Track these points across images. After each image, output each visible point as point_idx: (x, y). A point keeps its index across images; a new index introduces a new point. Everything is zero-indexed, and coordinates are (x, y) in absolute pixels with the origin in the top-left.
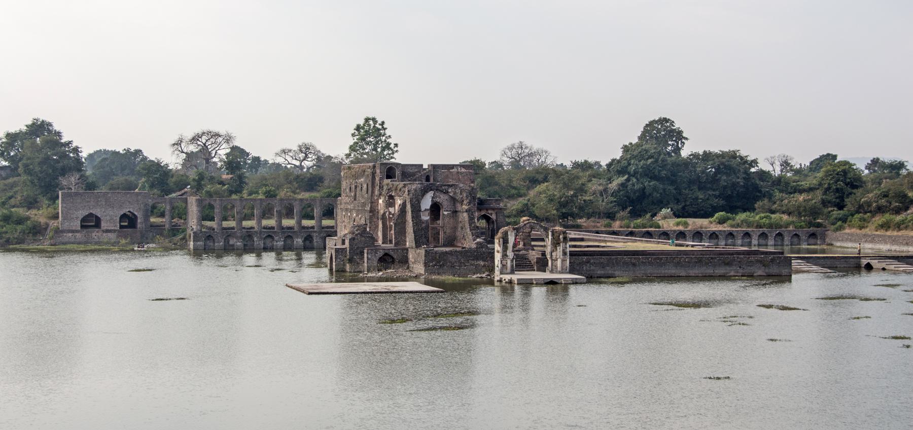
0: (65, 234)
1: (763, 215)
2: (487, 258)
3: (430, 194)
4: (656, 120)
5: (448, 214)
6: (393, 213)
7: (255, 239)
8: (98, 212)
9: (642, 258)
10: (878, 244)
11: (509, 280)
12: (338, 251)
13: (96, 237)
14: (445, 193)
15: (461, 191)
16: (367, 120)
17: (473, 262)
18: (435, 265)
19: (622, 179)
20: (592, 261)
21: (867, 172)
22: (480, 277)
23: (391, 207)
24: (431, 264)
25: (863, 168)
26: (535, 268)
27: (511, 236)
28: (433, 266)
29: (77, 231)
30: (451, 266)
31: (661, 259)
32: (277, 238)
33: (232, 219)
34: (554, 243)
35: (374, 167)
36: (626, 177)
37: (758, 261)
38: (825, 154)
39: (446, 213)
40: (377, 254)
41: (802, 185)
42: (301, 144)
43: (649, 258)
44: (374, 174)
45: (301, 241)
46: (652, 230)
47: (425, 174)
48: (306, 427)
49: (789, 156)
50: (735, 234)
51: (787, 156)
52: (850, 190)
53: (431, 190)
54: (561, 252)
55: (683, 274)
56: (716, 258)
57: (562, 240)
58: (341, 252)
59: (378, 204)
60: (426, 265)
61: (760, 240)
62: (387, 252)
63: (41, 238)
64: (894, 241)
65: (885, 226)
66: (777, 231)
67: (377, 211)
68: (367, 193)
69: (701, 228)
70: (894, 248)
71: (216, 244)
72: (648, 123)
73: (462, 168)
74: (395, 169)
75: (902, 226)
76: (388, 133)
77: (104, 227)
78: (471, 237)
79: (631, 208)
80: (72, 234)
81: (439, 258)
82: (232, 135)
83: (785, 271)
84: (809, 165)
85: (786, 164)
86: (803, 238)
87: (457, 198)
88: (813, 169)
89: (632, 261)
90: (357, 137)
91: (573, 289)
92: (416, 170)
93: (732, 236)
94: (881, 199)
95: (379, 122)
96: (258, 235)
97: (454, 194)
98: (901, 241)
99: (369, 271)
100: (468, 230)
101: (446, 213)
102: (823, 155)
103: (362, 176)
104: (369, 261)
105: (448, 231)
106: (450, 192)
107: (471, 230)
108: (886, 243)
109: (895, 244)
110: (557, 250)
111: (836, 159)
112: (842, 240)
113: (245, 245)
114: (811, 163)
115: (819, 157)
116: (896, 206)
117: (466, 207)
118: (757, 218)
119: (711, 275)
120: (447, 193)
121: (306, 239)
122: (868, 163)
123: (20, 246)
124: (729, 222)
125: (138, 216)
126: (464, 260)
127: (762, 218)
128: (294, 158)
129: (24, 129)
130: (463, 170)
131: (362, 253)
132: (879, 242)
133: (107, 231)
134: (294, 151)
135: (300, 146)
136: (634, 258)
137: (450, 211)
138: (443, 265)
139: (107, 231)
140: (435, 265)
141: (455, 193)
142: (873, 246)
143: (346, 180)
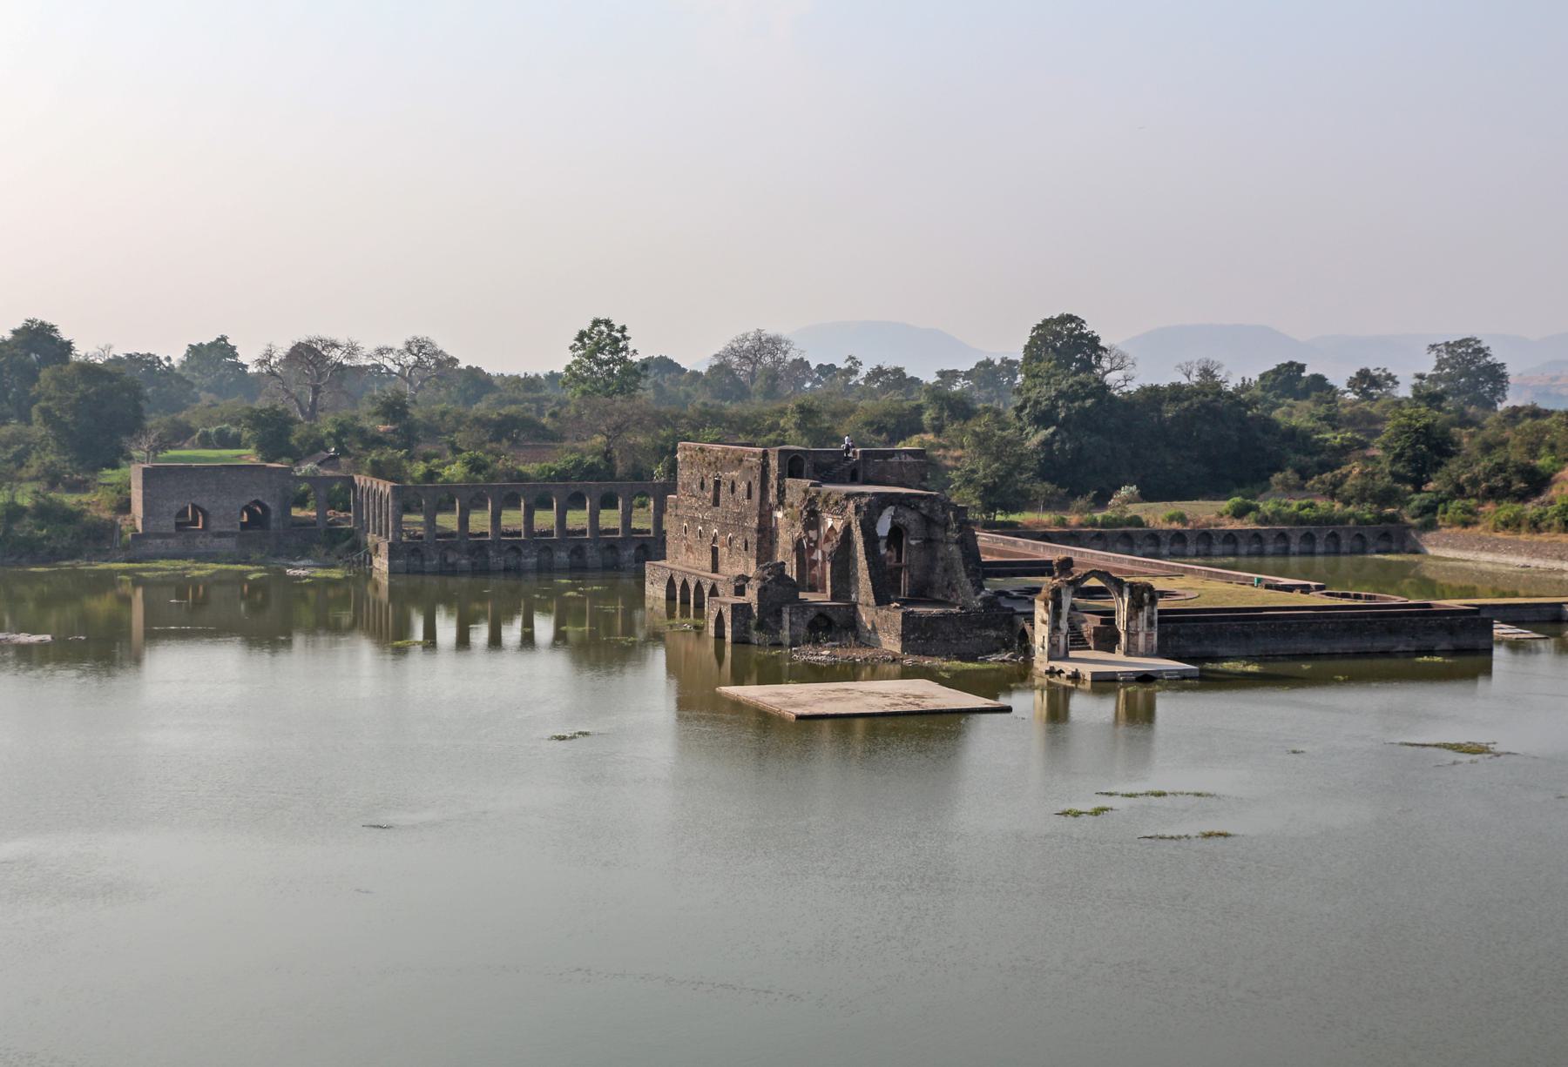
0: (150, 541)
1: (1304, 502)
2: (1001, 624)
4: (1055, 317)
5: (917, 544)
6: (815, 539)
7: (491, 553)
8: (204, 502)
9: (1261, 624)
10: (1505, 556)
11: (1073, 672)
12: (737, 608)
13: (201, 546)
14: (912, 509)
15: (943, 508)
16: (596, 323)
17: (978, 632)
18: (919, 638)
19: (1044, 434)
20: (1182, 631)
21: (1351, 396)
22: (1001, 661)
23: (813, 530)
24: (912, 637)
25: (1341, 385)
26: (1092, 644)
27: (1066, 595)
28: (915, 640)
29: (169, 536)
30: (945, 640)
31: (1290, 626)
32: (527, 551)
33: (419, 509)
34: (1133, 605)
35: (765, 454)
36: (1051, 430)
37: (1441, 626)
38: (1286, 362)
39: (913, 543)
40: (806, 614)
41: (1327, 440)
42: (411, 340)
43: (1271, 624)
44: (765, 468)
45: (566, 557)
46: (1132, 531)
47: (850, 466)
49: (1216, 361)
50: (1264, 535)
51: (1213, 362)
52: (1437, 458)
53: (892, 504)
54: (1145, 621)
55: (1324, 650)
56: (1375, 622)
57: (1147, 601)
58: (742, 610)
59: (771, 519)
60: (904, 638)
61: (1302, 545)
62: (822, 610)
63: (108, 547)
64: (1534, 551)
65: (1513, 524)
66: (1329, 529)
67: (769, 529)
68: (749, 497)
69: (1210, 525)
70: (1536, 562)
71: (427, 563)
72: (1041, 323)
73: (907, 456)
74: (802, 460)
75: (1542, 525)
76: (631, 346)
77: (214, 527)
78: (969, 587)
79: (1095, 492)
80: (161, 541)
81: (926, 625)
82: (357, 345)
83: (1482, 643)
84: (1257, 379)
86: (1371, 540)
87: (936, 518)
88: (1267, 388)
89: (1245, 630)
90: (581, 352)
92: (833, 460)
93: (1257, 539)
94: (1493, 475)
95: (617, 327)
96: (496, 546)
97: (930, 512)
98: (1548, 553)
100: (963, 574)
101: (913, 543)
102: (1283, 364)
103: (735, 469)
104: (793, 627)
105: (916, 573)
106: (922, 509)
107: (968, 576)
108: (1519, 554)
109: (1537, 557)
110: (1137, 617)
111: (1304, 371)
112: (1437, 545)
113: (474, 564)
114: (1263, 377)
115: (1275, 367)
116: (1520, 489)
117: (956, 536)
118: (1295, 504)
119: (1367, 650)
120: (917, 508)
121: (573, 552)
122: (1351, 378)
124: (1252, 514)
125: (272, 508)
126: (965, 629)
127: (1302, 508)
128: (397, 362)
129: (8, 336)
130: (910, 459)
131: (779, 613)
132: (1508, 552)
133: (220, 535)
134: (398, 351)
135: (409, 343)
136: (1248, 625)
137: (921, 539)
138: (932, 637)
139: (220, 535)
140: (919, 638)
141: (932, 510)
142: (1496, 558)
143: (691, 468)
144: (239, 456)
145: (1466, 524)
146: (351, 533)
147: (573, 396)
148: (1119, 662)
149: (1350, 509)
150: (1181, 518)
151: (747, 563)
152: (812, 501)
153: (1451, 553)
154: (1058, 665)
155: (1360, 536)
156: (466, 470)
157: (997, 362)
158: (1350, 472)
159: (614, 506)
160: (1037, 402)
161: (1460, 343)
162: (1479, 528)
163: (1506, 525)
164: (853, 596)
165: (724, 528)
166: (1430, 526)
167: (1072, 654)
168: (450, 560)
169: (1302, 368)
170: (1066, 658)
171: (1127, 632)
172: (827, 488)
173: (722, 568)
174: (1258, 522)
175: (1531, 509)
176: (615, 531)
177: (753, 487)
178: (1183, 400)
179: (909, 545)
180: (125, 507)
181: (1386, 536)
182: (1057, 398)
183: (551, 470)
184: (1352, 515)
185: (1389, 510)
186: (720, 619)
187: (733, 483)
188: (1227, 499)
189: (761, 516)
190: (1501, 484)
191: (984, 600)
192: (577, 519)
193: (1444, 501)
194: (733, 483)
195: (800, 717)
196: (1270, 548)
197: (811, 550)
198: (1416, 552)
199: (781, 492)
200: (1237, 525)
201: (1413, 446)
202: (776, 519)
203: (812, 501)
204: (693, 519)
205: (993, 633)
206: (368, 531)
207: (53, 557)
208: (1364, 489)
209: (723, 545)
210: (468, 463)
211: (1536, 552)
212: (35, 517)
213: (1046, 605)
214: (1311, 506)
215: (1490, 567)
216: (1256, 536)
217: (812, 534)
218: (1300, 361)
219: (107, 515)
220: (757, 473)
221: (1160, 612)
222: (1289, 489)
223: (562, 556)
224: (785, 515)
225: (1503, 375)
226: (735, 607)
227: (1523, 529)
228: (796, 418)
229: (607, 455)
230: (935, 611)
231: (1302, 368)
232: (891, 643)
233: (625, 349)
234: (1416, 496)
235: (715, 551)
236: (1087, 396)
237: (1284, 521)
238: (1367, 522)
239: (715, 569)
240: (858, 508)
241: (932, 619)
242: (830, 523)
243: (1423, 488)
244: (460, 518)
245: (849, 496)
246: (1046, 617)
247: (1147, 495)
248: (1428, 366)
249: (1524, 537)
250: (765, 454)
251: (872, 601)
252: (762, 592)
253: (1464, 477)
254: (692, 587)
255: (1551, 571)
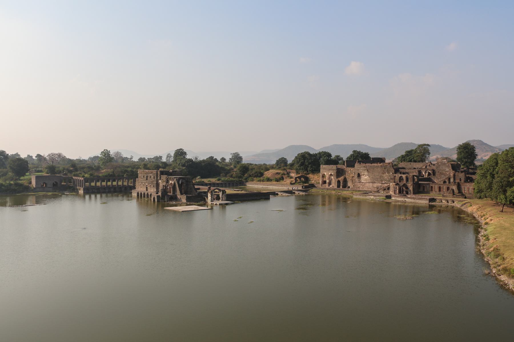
1: (228, 178)
3: (181, 180)
35: (157, 171)
36: (185, 167)
48: (44, 210)
60: (186, 200)
65: (260, 181)
68: (154, 178)
75: (264, 181)
78: (195, 191)
85: (196, 158)
91: (227, 207)
99: (6, 168)
103: (151, 174)
108: (261, 185)
118: (227, 178)
123: (46, 193)
127: (228, 179)
130: (179, 172)
131: (164, 197)
132: (259, 185)
133: (49, 188)
139: (49, 188)
144: (42, 174)
145: (252, 181)
146: (72, 187)
147: (101, 163)
148: (220, 202)
149: (235, 179)
150: (210, 181)
151: (154, 189)
152: (167, 179)
153: (251, 186)
154: (213, 203)
155: (237, 183)
156: (89, 175)
157: (158, 156)
158: (233, 174)
159: (115, 181)
160: (182, 163)
161: (235, 153)
162: (254, 182)
163: (259, 181)
164: (176, 194)
165: (149, 184)
166: (247, 181)
167: (214, 201)
168: (93, 191)
169: (213, 157)
170: (213, 202)
171: (222, 197)
172: (169, 176)
173: (148, 190)
174: (222, 181)
175: (262, 178)
176: (121, 185)
177: (155, 177)
178: (205, 162)
179: (184, 185)
180: (30, 183)
181: (240, 183)
182: (185, 162)
183: (104, 175)
184: (235, 180)
185: (240, 179)
186: (154, 198)
187: (150, 176)
188: (216, 178)
189: (156, 181)
190: (256, 175)
191: (198, 193)
192: (109, 183)
193: (248, 178)
194: (150, 176)
195: (182, 211)
196: (224, 186)
197: (167, 186)
198: (245, 186)
199: (160, 178)
200: (218, 182)
201: (243, 169)
202: (159, 182)
203: (167, 179)
204: (142, 182)
205: (199, 198)
206: (77, 186)
207: (19, 192)
208: (237, 176)
209: (149, 186)
210: (90, 174)
211: (264, 185)
212: (14, 185)
213: (210, 193)
214: (229, 179)
215: (257, 187)
216: (221, 184)
217: (167, 184)
218: (213, 156)
219: (27, 185)
220: (156, 174)
221: (227, 194)
222: (223, 176)
223: (112, 190)
224: (161, 181)
225: (242, 158)
226: (157, 196)
227: (261, 181)
228: (143, 166)
229: (113, 172)
230: (191, 195)
231: (213, 157)
232: (184, 201)
233: (110, 155)
234: (244, 177)
235: (147, 188)
236: (190, 162)
237: (225, 181)
238: (238, 181)
239: (147, 190)
240: (176, 180)
241: (191, 196)
242: (171, 182)
243: (244, 176)
244: (117, 182)
245: (175, 178)
246: (210, 195)
247: (202, 178)
248: (231, 157)
249: (262, 183)
250: (157, 171)
251: (180, 194)
252: (162, 193)
253: (251, 174)
254: (143, 193)
255: (266, 188)
